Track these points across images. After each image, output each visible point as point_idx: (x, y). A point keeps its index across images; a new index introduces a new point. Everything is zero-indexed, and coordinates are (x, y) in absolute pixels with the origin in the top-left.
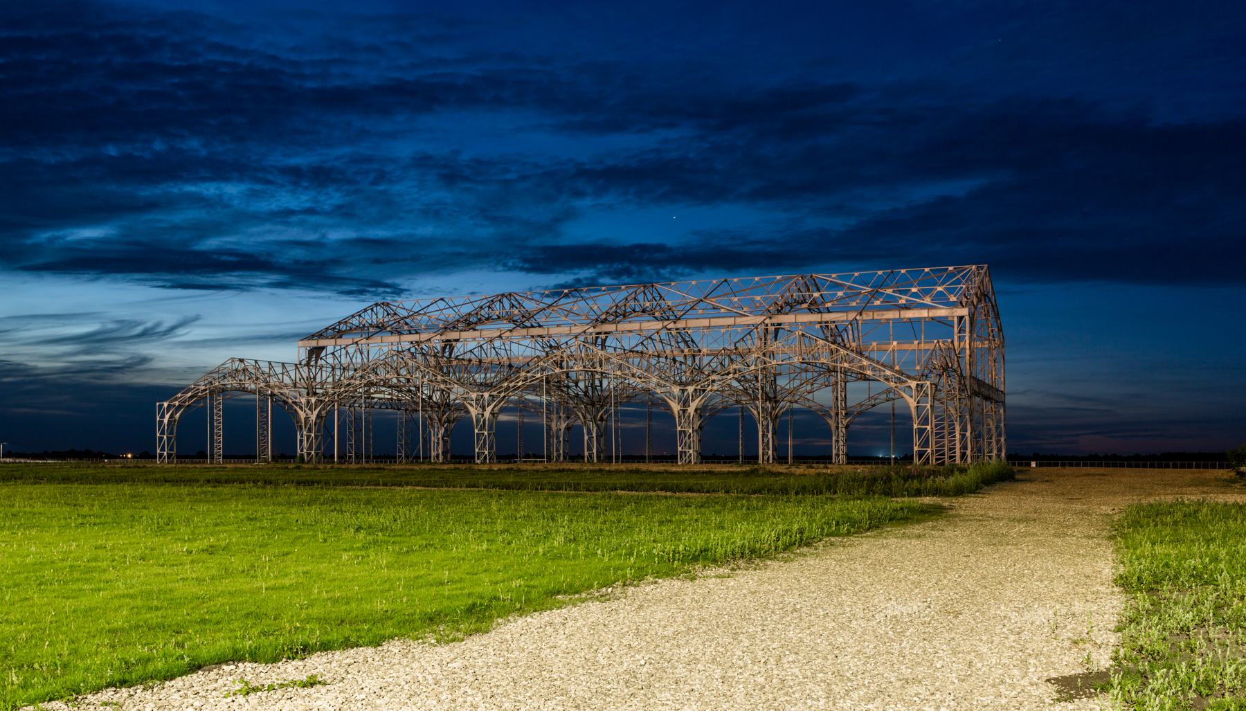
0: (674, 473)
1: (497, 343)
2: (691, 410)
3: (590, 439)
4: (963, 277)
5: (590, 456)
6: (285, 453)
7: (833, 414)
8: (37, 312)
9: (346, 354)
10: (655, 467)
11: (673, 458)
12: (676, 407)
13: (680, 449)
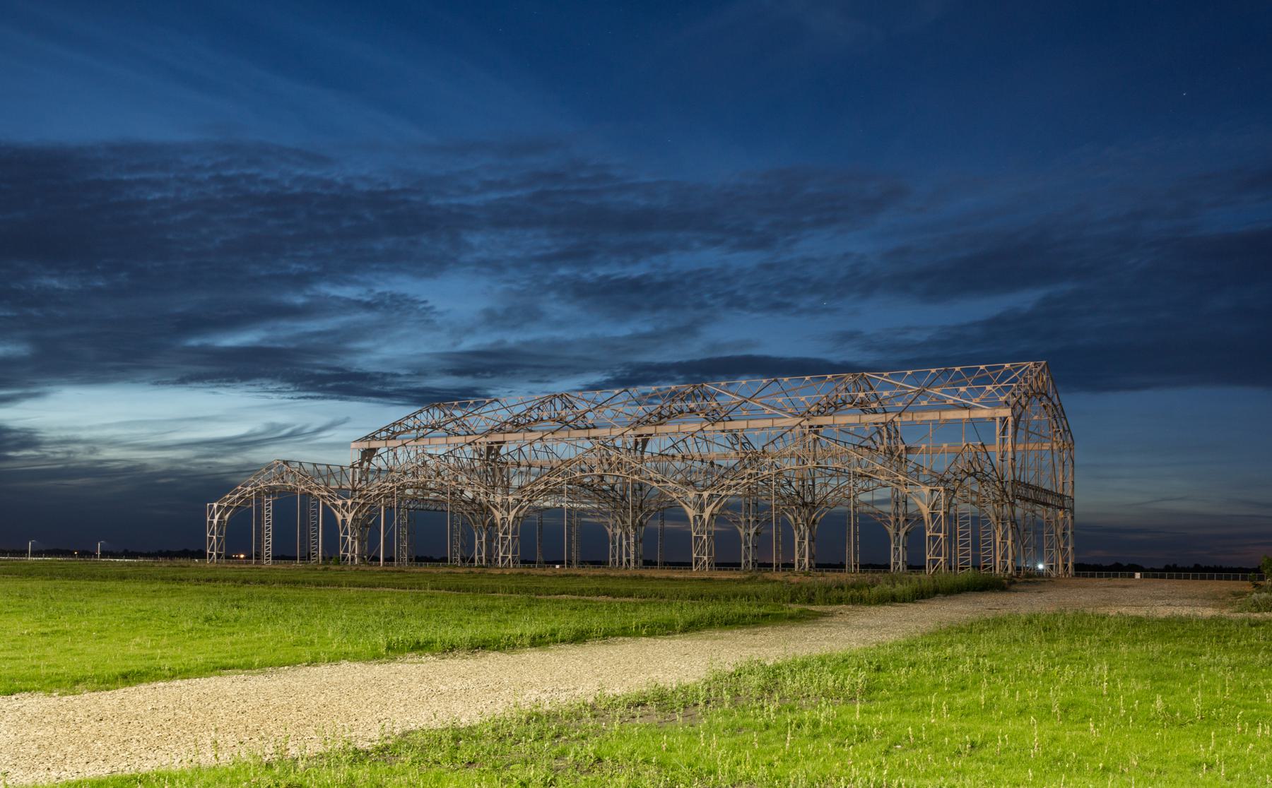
0: (677, 579)
1: (537, 446)
2: (706, 515)
3: (628, 544)
4: (1020, 375)
5: (481, 559)
6: (332, 553)
7: (892, 519)
8: (200, 414)
9: (398, 457)
10: (665, 573)
11: (688, 565)
12: (691, 513)
13: (695, 555)
